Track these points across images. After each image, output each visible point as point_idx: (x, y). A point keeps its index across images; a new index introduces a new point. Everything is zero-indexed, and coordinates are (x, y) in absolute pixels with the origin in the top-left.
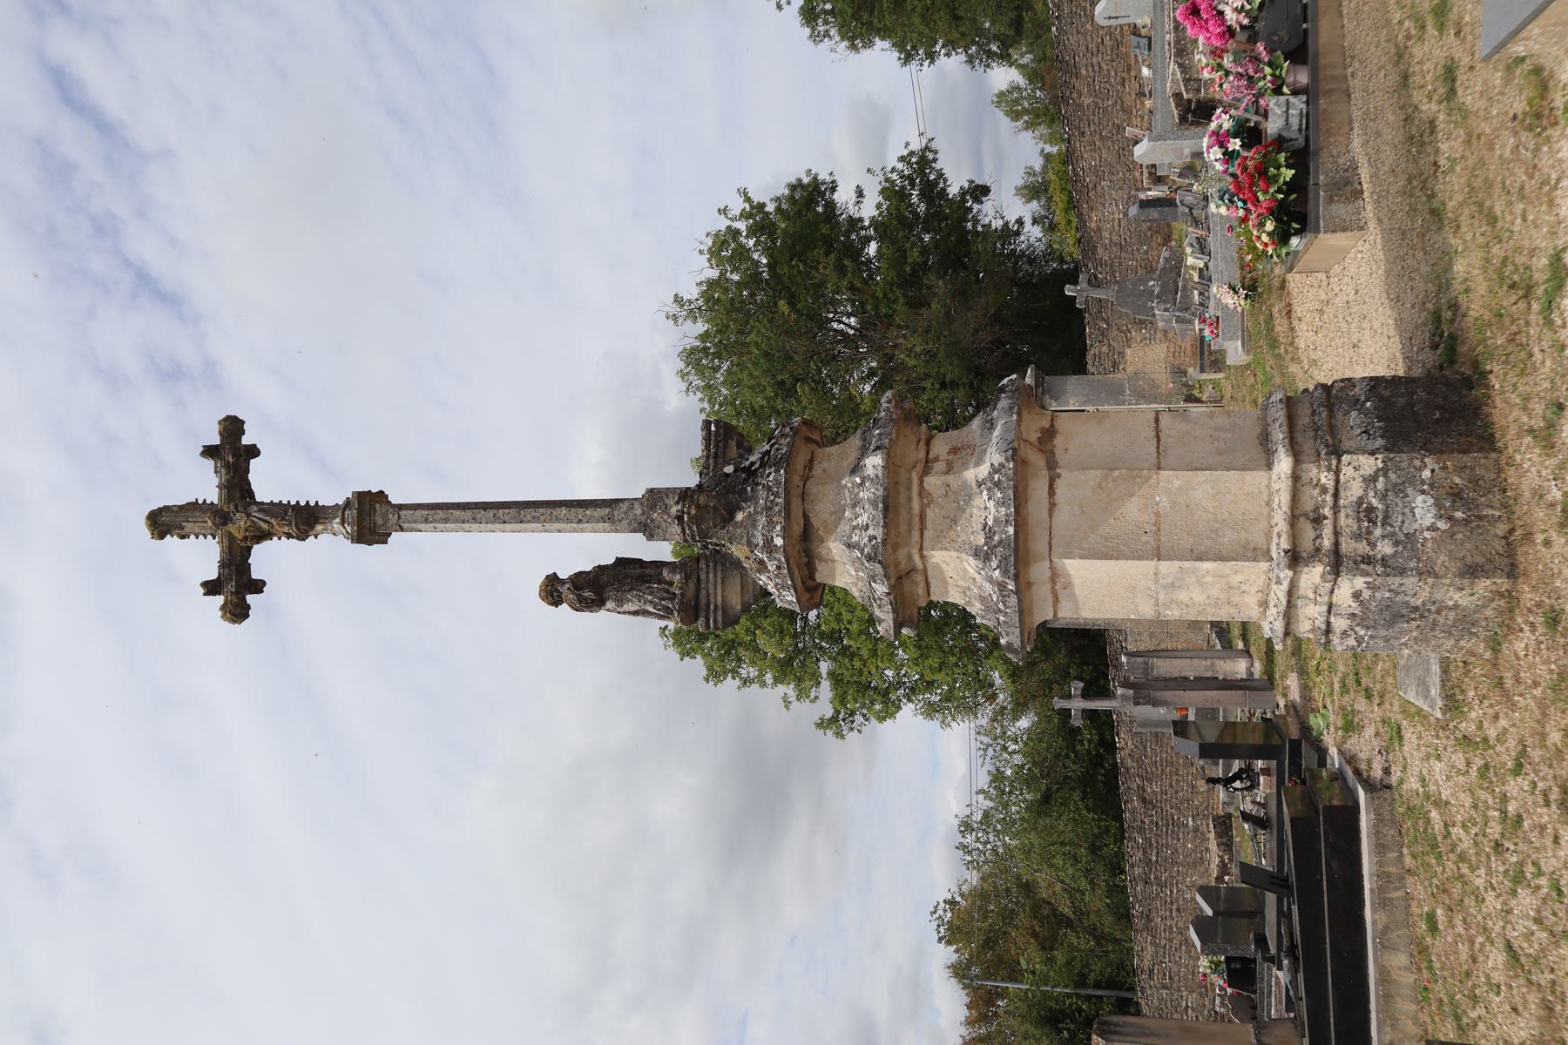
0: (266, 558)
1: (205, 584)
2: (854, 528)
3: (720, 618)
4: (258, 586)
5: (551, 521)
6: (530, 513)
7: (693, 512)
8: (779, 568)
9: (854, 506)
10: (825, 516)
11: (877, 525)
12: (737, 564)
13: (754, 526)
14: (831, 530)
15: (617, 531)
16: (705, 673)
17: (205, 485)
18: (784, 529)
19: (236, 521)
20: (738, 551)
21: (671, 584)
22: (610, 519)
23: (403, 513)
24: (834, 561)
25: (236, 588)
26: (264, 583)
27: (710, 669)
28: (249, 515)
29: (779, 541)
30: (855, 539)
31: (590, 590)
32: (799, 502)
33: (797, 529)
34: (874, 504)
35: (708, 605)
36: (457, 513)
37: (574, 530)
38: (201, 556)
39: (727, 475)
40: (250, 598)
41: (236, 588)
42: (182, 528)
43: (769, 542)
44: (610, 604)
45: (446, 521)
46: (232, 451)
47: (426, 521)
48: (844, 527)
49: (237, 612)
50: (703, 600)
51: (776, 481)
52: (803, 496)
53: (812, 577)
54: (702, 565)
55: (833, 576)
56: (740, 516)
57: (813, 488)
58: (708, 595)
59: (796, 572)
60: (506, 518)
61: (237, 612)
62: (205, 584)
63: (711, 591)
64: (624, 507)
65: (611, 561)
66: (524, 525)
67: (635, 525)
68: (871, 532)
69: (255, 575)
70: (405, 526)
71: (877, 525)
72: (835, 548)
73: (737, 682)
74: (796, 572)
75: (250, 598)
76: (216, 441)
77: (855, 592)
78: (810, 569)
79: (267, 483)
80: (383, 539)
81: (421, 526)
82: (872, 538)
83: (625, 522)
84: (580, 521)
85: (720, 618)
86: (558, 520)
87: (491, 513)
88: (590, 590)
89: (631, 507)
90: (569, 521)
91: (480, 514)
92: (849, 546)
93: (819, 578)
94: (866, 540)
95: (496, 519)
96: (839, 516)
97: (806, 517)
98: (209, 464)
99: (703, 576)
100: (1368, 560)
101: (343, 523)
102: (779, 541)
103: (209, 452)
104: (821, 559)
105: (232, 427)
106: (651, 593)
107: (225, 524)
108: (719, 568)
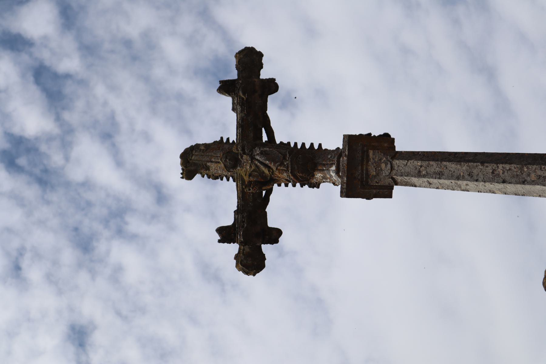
0: (285, 204)
1: (221, 231)
4: (274, 236)
17: (221, 121)
19: (254, 162)
23: (396, 162)
25: (251, 238)
26: (279, 232)
28: (253, 158)
36: (452, 166)
38: (223, 198)
40: (266, 248)
41: (251, 238)
42: (208, 168)
45: (440, 175)
46: (249, 85)
47: (419, 175)
49: (251, 262)
60: (507, 176)
61: (251, 262)
62: (221, 231)
66: (528, 187)
69: (271, 223)
70: (399, 179)
75: (266, 248)
76: (233, 75)
79: (289, 126)
80: (386, 192)
81: (414, 180)
87: (489, 168)
95: (495, 178)
98: (227, 101)
100: (327, 164)
101: (337, 172)
103: (226, 87)
105: (250, 59)
107: (234, 167)
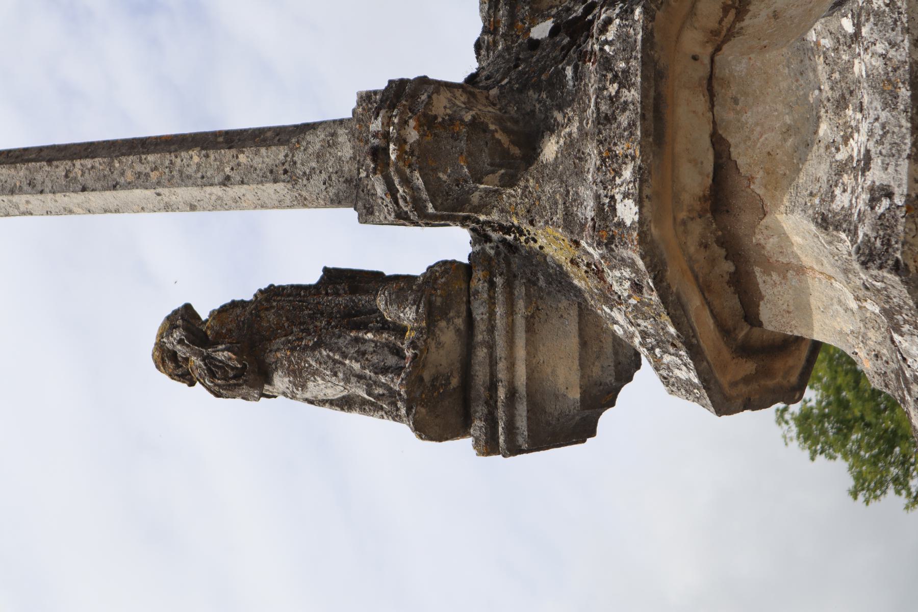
2: (841, 168)
3: (522, 423)
5: (171, 183)
6: (130, 165)
7: (413, 135)
8: (637, 287)
9: (841, 104)
10: (771, 139)
11: (894, 153)
12: (559, 280)
13: (579, 173)
14: (784, 175)
15: (303, 202)
16: (850, 483)
18: (641, 175)
20: (551, 243)
21: (400, 331)
22: (285, 174)
24: (801, 270)
27: (859, 478)
29: (628, 212)
30: (842, 200)
31: (231, 348)
32: (700, 103)
33: (694, 180)
34: (885, 89)
35: (492, 387)
37: (219, 205)
39: (535, 44)
43: (605, 212)
44: (281, 381)
48: (817, 169)
50: (481, 374)
51: (623, 38)
52: (711, 86)
53: (751, 318)
54: (479, 283)
55: (804, 310)
56: (551, 149)
57: (736, 61)
58: (493, 362)
59: (695, 302)
63: (501, 351)
64: (316, 141)
65: (312, 277)
66: (122, 194)
67: (338, 186)
68: (876, 175)
71: (894, 153)
72: (792, 229)
73: (903, 500)
74: (695, 302)
77: (866, 365)
78: (744, 288)
82: (883, 192)
83: (317, 181)
84: (226, 181)
85: (522, 423)
86: (185, 179)
87: (61, 168)
88: (231, 348)
89: (331, 143)
90: (205, 182)
91: (43, 171)
92: (825, 222)
93: (774, 318)
94: (862, 204)
95: (71, 184)
96: (803, 138)
97: (719, 144)
99: (480, 312)
102: (628, 212)
104: (768, 266)
106: (361, 355)
108: (520, 290)
